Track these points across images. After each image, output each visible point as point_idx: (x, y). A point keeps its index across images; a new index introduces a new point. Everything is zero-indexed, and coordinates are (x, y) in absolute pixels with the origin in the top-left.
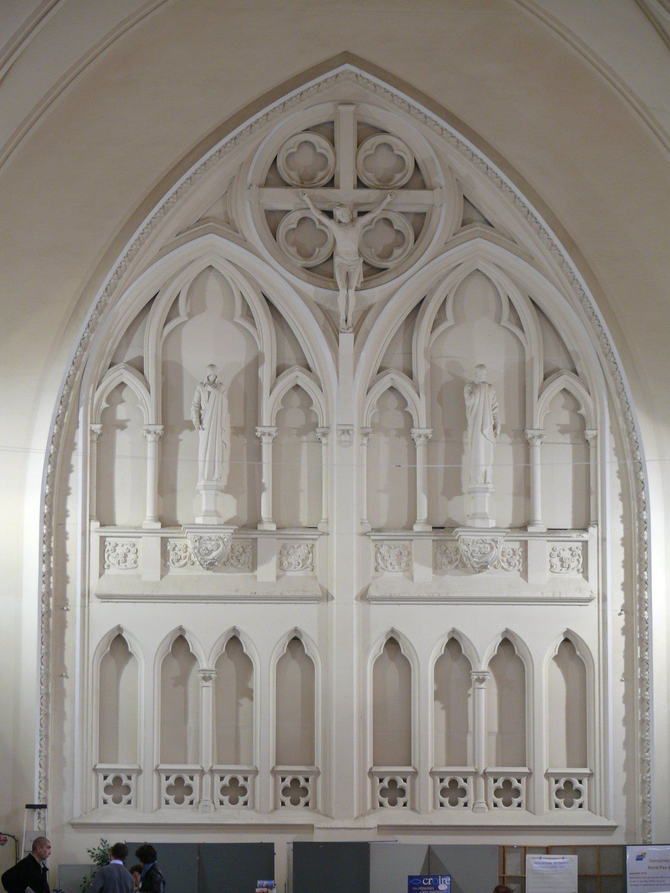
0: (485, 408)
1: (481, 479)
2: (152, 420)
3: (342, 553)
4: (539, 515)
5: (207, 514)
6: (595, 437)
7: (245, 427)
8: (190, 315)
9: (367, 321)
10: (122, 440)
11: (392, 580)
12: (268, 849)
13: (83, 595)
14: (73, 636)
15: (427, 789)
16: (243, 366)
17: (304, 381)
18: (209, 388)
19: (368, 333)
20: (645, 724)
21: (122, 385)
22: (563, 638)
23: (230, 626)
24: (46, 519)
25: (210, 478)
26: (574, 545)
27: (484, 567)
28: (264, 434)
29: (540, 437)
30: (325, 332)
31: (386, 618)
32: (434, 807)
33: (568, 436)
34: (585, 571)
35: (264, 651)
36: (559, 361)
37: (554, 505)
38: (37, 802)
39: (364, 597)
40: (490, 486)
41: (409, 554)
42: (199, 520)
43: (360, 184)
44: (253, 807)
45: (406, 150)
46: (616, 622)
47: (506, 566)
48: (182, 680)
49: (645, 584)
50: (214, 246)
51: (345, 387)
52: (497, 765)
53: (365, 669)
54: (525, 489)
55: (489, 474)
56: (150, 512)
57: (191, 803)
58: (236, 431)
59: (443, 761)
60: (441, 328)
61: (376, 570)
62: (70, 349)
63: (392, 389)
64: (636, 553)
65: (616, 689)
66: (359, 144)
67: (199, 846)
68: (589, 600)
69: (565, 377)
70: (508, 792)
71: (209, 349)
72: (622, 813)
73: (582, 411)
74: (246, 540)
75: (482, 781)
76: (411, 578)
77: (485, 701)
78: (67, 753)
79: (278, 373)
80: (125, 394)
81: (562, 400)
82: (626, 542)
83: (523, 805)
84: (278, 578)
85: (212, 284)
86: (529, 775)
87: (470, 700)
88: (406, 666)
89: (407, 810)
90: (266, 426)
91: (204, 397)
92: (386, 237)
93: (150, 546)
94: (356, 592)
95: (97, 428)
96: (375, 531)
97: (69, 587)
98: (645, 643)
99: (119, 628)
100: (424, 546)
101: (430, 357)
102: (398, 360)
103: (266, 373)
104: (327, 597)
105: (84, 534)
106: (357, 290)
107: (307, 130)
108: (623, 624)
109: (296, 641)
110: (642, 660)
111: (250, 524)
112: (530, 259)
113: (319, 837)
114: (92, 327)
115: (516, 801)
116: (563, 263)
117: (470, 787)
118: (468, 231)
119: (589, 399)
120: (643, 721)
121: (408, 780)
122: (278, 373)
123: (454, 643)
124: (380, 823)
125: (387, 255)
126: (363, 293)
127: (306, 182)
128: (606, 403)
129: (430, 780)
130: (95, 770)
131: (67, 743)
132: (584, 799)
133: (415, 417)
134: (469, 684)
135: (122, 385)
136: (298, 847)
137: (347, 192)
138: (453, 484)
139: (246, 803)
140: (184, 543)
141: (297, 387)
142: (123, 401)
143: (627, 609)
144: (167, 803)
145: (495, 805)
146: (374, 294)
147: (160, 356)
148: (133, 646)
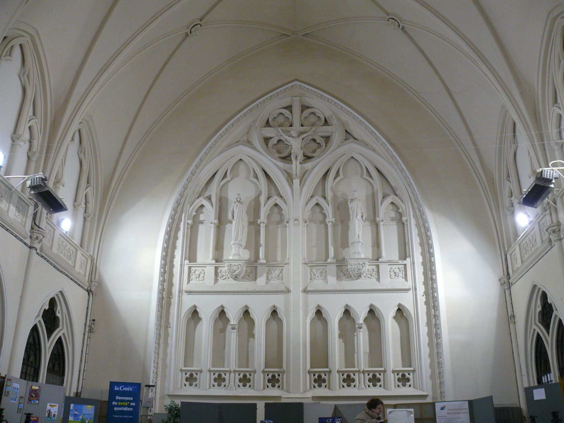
1: (357, 237)
2: (213, 218)
3: (295, 272)
4: (384, 254)
5: (234, 255)
6: (407, 220)
7: (254, 223)
8: (232, 179)
9: (305, 176)
10: (201, 228)
11: (318, 284)
13: (179, 292)
15: (336, 379)
16: (254, 197)
17: (279, 201)
18: (237, 203)
19: (305, 181)
20: (439, 345)
21: (202, 206)
22: (397, 308)
23: (244, 305)
25: (236, 240)
26: (400, 266)
27: (359, 276)
28: (261, 223)
29: (382, 221)
30: (288, 181)
31: (315, 300)
32: (340, 388)
33: (395, 222)
34: (406, 278)
35: (260, 317)
36: (388, 191)
38: (151, 384)
39: (305, 291)
40: (361, 240)
41: (326, 272)
42: (231, 258)
44: (254, 388)
45: (320, 113)
46: (422, 299)
47: (370, 276)
48: (223, 330)
49: (434, 281)
50: (243, 151)
51: (297, 204)
52: (369, 367)
53: (306, 323)
54: (377, 244)
55: (361, 236)
56: (211, 256)
57: (225, 386)
58: (250, 223)
59: (344, 365)
60: (338, 179)
61: (311, 279)
62: (179, 189)
63: (317, 204)
64: (428, 268)
65: (424, 330)
66: (302, 112)
67: (220, 404)
68: (409, 290)
69: (390, 197)
70: (374, 380)
71: (240, 191)
72: (430, 388)
73: (400, 210)
74: (252, 269)
75: (362, 375)
76: (327, 282)
77: (362, 338)
78: (168, 362)
79: (268, 198)
80: (204, 210)
81: (391, 207)
82: (424, 264)
83: (382, 386)
84: (266, 283)
86: (384, 371)
87: (356, 338)
88: (325, 322)
89: (326, 390)
90: (265, 222)
91: (235, 207)
93: (210, 271)
94: (301, 289)
95: (190, 222)
97: (173, 288)
98: (436, 307)
99: (195, 306)
103: (262, 199)
104: (288, 291)
105: (181, 265)
106: (301, 163)
108: (425, 300)
109: (274, 312)
110: (435, 315)
112: (374, 150)
113: (283, 401)
114: (189, 181)
115: (378, 384)
116: (388, 150)
117: (356, 377)
118: (347, 142)
119: (403, 205)
120: (437, 344)
121: (327, 375)
122: (268, 198)
123: (347, 312)
124: (314, 395)
125: (314, 151)
126: (304, 165)
128: (410, 206)
129: (337, 375)
130: (181, 370)
131: (168, 358)
132: (411, 382)
133: (327, 215)
134: (355, 330)
135: (202, 206)
136: (267, 405)
138: (344, 242)
139: (250, 386)
140: (224, 269)
141: (276, 205)
142: (203, 213)
143: (426, 293)
144: (214, 386)
145: (369, 386)
146: (308, 165)
147: (219, 193)
148: (201, 314)
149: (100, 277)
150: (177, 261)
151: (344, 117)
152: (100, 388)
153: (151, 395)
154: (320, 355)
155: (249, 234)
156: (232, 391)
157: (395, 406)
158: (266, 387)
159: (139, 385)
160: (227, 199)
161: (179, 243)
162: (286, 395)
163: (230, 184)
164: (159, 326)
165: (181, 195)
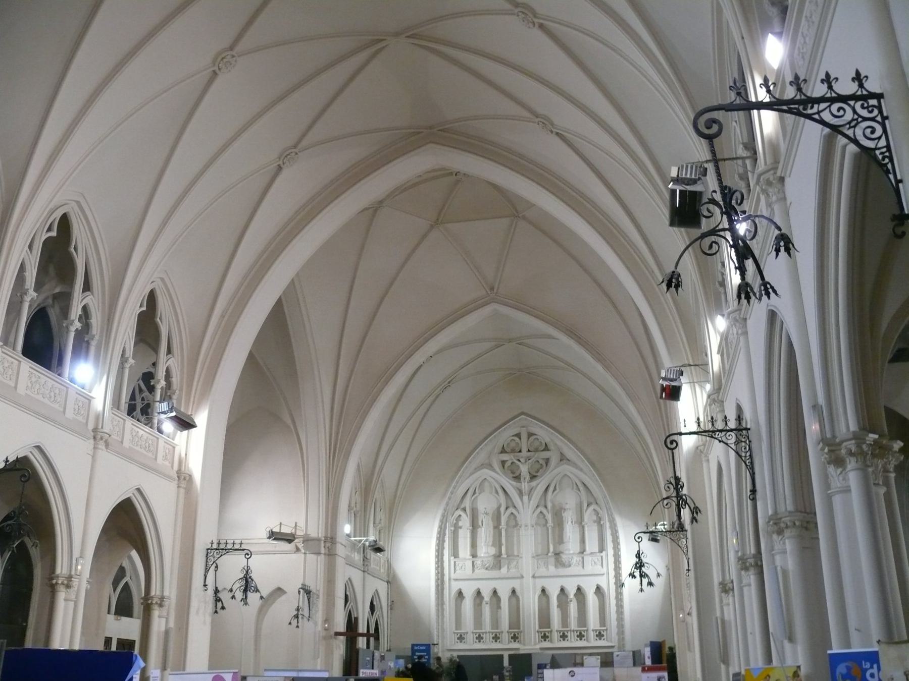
0: (569, 517)
4: (587, 548)
7: (497, 527)
10: (460, 531)
11: (542, 571)
12: (502, 656)
14: (446, 592)
15: (556, 636)
17: (514, 511)
21: (460, 516)
24: (437, 557)
27: (570, 566)
31: (540, 583)
35: (504, 596)
36: (592, 500)
37: (592, 545)
39: (534, 577)
43: (529, 451)
46: (612, 581)
48: (480, 604)
50: (486, 473)
51: (527, 513)
54: (583, 541)
65: (613, 602)
67: (481, 656)
70: (581, 636)
71: (486, 503)
74: (498, 561)
77: (573, 608)
79: (507, 508)
85: (486, 484)
88: (548, 597)
90: (504, 526)
92: (537, 466)
93: (469, 564)
96: (537, 556)
100: (552, 560)
101: (552, 502)
102: (543, 503)
103: (502, 509)
104: (522, 577)
107: (789, 338)
109: (514, 592)
111: (498, 556)
112: (581, 470)
113: (522, 652)
114: (450, 498)
117: (569, 634)
122: (507, 508)
123: (562, 589)
125: (537, 471)
127: (513, 451)
136: (510, 656)
137: (524, 453)
138: (560, 539)
146: (534, 483)
149: (394, 572)
150: (446, 558)
151: (559, 443)
152: (406, 647)
153: (436, 650)
154: (545, 619)
155: (494, 536)
156: (488, 646)
157: (591, 654)
158: (509, 642)
159: (429, 645)
160: (477, 509)
161: (446, 545)
162: (523, 648)
163: (479, 498)
164: (437, 605)
165: (445, 510)
